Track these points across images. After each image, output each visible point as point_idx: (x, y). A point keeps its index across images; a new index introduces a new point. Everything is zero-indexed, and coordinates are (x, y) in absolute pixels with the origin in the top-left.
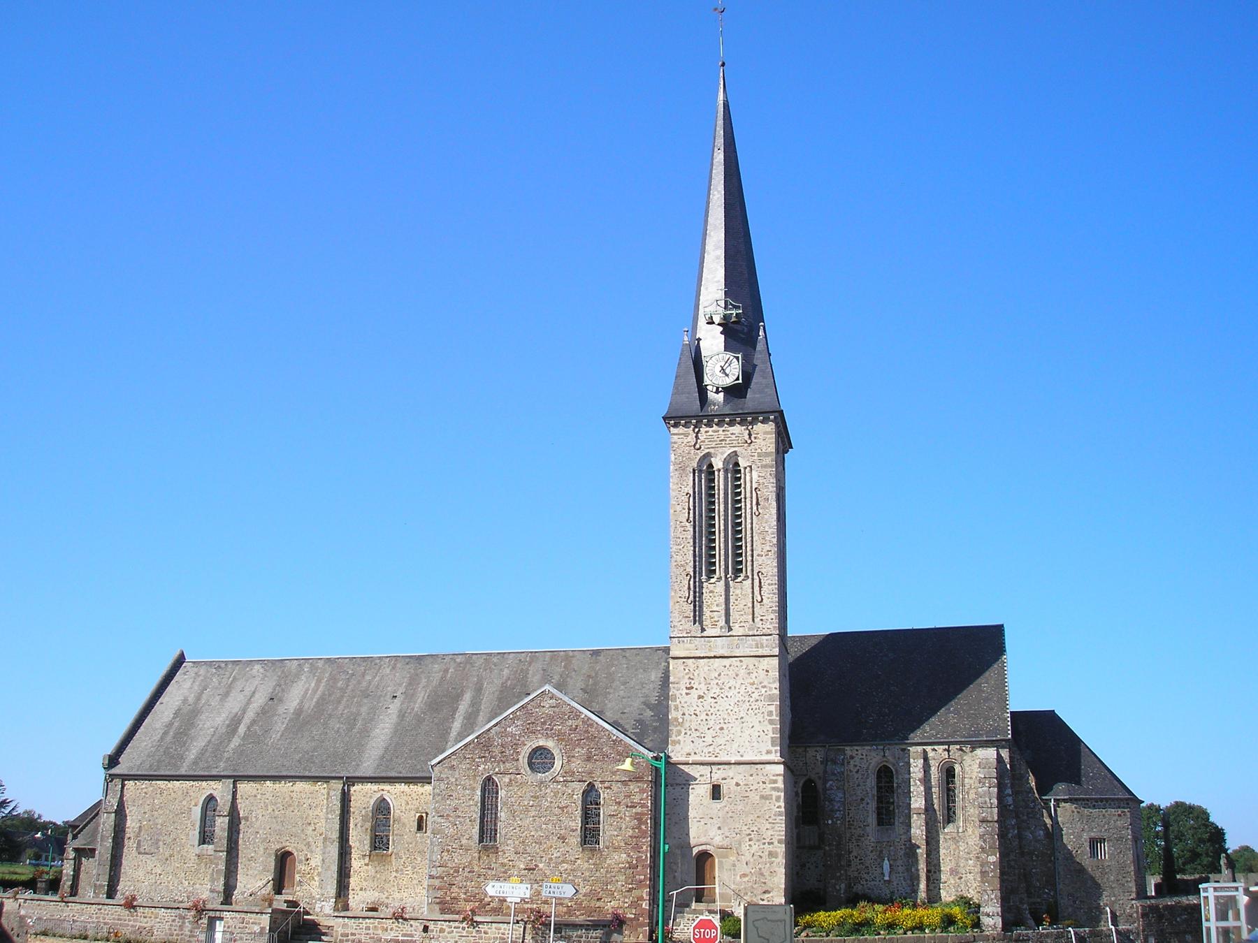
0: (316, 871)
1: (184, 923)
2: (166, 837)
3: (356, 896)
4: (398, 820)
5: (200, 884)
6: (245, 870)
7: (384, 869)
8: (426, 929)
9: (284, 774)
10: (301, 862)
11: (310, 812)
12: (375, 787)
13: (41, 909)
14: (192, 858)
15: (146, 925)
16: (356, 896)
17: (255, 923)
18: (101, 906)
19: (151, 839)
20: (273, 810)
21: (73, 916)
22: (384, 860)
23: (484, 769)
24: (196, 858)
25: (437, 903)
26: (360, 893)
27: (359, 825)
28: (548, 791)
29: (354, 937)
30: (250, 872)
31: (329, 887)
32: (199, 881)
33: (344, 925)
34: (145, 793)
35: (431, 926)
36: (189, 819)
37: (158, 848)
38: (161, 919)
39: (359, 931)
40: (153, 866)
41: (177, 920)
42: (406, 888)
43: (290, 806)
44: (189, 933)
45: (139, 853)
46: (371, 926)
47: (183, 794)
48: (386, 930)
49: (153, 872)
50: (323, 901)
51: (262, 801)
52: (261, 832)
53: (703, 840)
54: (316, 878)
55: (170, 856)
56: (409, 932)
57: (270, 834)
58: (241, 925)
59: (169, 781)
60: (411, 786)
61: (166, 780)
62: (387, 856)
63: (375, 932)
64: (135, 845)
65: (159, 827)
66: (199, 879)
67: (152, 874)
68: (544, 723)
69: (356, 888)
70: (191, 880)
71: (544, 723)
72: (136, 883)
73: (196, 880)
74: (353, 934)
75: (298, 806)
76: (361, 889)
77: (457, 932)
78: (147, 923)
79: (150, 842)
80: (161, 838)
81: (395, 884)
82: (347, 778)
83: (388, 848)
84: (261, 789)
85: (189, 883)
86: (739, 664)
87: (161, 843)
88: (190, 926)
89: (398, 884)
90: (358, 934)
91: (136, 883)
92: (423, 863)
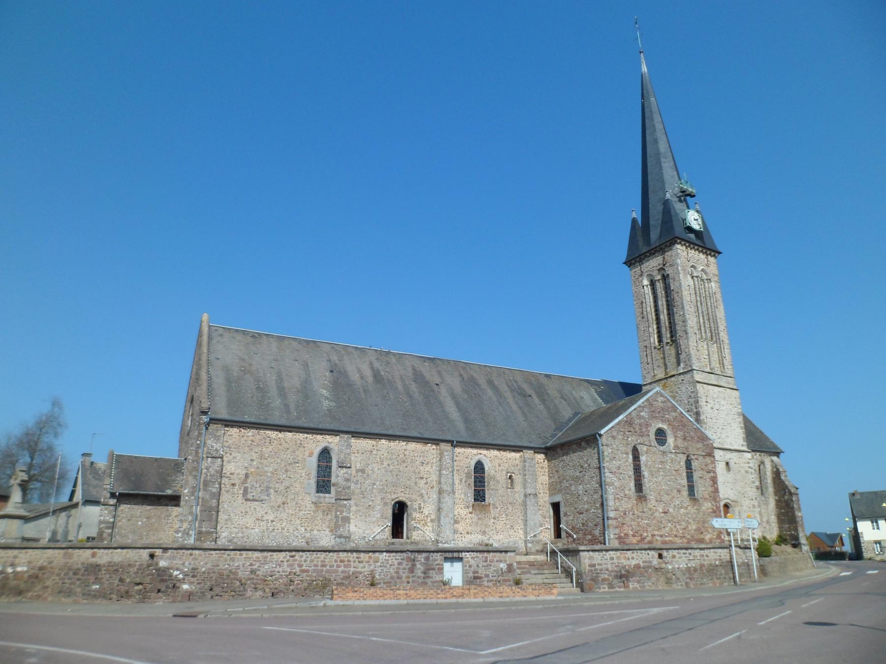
0: (429, 518)
1: (414, 565)
2: (277, 485)
3: (463, 539)
4: (494, 478)
5: (318, 530)
6: (363, 517)
7: (485, 517)
8: (660, 556)
9: (398, 433)
10: (415, 510)
11: (422, 468)
12: (475, 451)
13: (194, 559)
14: (308, 505)
15: (363, 570)
16: (463, 539)
17: (501, 561)
18: (294, 553)
19: (260, 486)
20: (389, 465)
21: (251, 565)
22: (485, 509)
23: (633, 439)
24: (312, 506)
25: (617, 538)
26: (467, 536)
27: (464, 480)
28: (668, 458)
29: (601, 567)
30: (368, 519)
31: (447, 531)
32: (317, 527)
33: (591, 558)
34: (252, 441)
35: (665, 553)
36: (303, 469)
37: (268, 495)
38: (383, 563)
39: (605, 561)
40: (263, 512)
41: (405, 563)
42: (503, 531)
43: (404, 462)
44: (423, 575)
45: (247, 500)
46: (614, 556)
47: (296, 444)
48: (629, 559)
49: (264, 519)
50: (445, 543)
51: (378, 457)
52: (377, 483)
53: (726, 496)
54: (429, 524)
55: (284, 503)
56: (648, 560)
57: (387, 486)
58: (485, 564)
59: (280, 431)
60: (502, 452)
61: (276, 430)
62: (486, 506)
63: (619, 562)
64: (241, 492)
65: (269, 474)
66: (316, 525)
67: (262, 520)
68: (659, 412)
69: (463, 532)
70: (308, 526)
71: (659, 412)
72: (244, 530)
73: (314, 527)
74: (599, 564)
75: (411, 462)
76: (468, 533)
77: (685, 557)
78: (364, 567)
79: (259, 490)
80: (272, 485)
81: (494, 528)
82: (457, 442)
83: (484, 500)
84: (377, 446)
85: (306, 530)
86: (724, 391)
87: (272, 491)
88: (422, 568)
89: (496, 528)
90: (605, 564)
91: (244, 530)
92: (513, 512)
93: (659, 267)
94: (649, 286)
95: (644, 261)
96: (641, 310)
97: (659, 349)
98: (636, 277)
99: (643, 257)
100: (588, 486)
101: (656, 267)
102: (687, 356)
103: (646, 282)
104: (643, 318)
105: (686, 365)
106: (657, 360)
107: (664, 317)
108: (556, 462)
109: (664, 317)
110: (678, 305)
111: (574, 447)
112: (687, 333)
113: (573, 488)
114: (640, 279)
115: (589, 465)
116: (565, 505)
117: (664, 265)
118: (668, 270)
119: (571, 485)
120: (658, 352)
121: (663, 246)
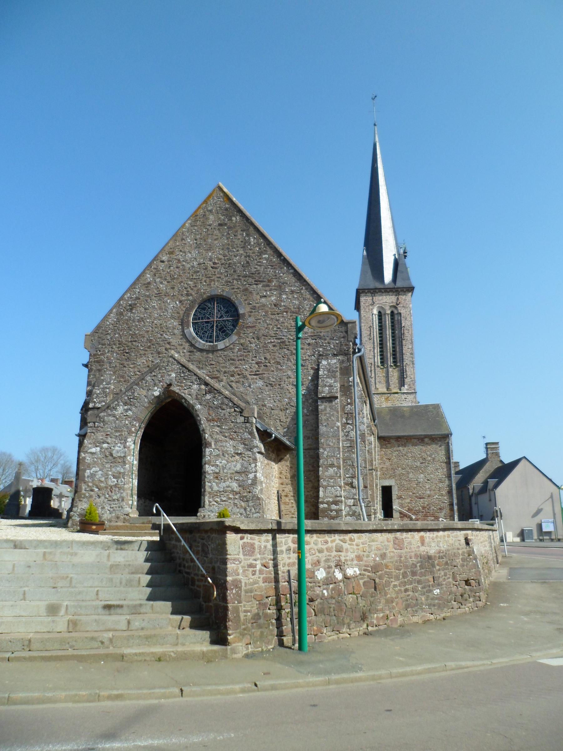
93: (391, 304)
94: (377, 316)
95: (376, 294)
96: (369, 333)
97: (381, 369)
98: (367, 305)
99: (377, 291)
100: (432, 476)
101: (389, 303)
102: (412, 381)
103: (375, 312)
104: (370, 339)
105: (410, 388)
106: (379, 377)
107: (389, 344)
108: (389, 451)
109: (389, 344)
110: (407, 340)
111: (392, 441)
112: (413, 364)
113: (411, 475)
114: (371, 307)
115: (434, 459)
116: (399, 490)
117: (397, 304)
118: (401, 310)
119: (408, 473)
120: (381, 370)
121: (399, 290)
